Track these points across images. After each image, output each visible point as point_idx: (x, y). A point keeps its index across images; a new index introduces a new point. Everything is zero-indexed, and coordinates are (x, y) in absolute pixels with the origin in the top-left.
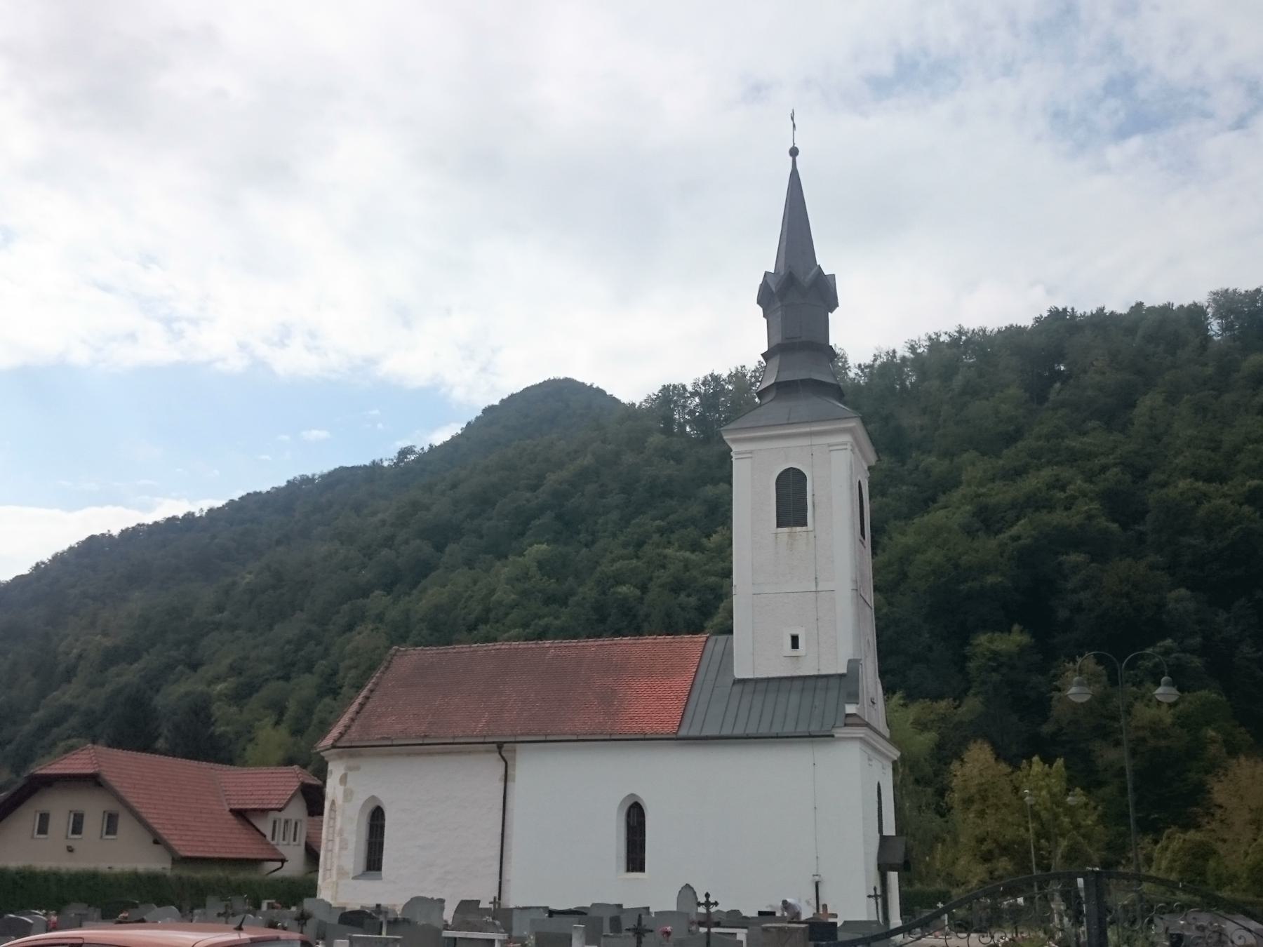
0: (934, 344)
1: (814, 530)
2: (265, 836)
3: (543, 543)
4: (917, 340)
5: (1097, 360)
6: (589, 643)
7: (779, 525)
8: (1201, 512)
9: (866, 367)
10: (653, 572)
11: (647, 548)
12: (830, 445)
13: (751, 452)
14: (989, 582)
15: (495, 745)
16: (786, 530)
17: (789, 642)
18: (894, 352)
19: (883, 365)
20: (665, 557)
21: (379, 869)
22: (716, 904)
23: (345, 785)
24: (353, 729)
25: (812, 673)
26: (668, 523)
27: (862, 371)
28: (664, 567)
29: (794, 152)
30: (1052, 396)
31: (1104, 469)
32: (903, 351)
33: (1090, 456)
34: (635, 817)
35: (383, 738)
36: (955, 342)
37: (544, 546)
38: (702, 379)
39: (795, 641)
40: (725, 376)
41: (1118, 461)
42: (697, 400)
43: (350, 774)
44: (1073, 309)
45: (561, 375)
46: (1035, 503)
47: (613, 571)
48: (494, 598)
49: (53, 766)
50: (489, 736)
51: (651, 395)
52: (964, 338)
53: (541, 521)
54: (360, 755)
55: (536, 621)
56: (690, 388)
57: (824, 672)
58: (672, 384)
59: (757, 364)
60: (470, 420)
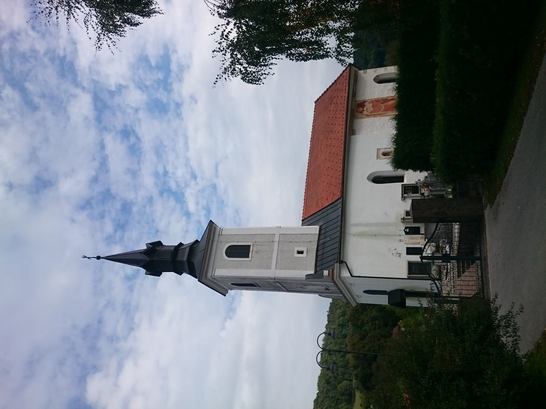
17: (300, 249)
29: (98, 258)
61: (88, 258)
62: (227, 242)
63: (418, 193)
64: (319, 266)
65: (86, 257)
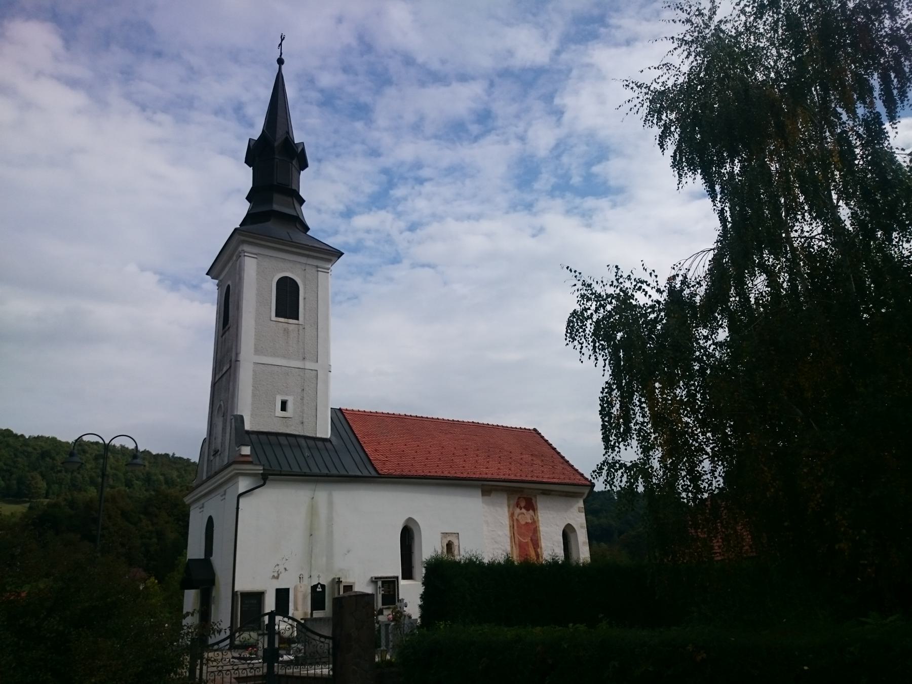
17: (290, 406)
29: (280, 61)
65: (282, 40)
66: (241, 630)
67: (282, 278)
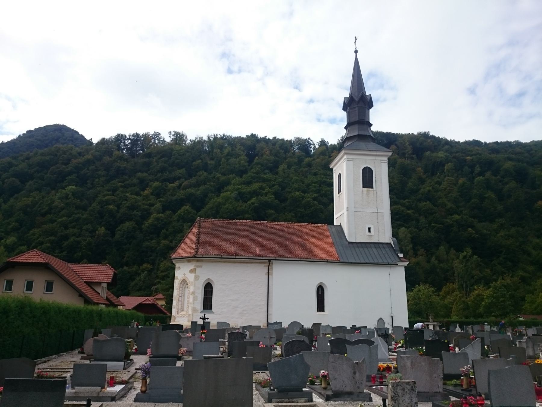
0: (216, 138)
1: (376, 190)
2: (99, 294)
3: (73, 186)
4: (211, 135)
5: (266, 152)
6: (282, 224)
7: (363, 187)
8: (304, 202)
9: (193, 141)
10: (122, 201)
11: (118, 192)
12: (381, 160)
13: (353, 159)
14: (246, 216)
15: (268, 261)
16: (366, 189)
17: (372, 230)
18: (202, 137)
19: (198, 141)
20: (127, 196)
21: (211, 308)
22: (208, 319)
23: (195, 273)
24: (200, 250)
25: (377, 242)
26: (125, 184)
27: (191, 142)
28: (126, 200)
29: (356, 52)
30: (255, 161)
31: (274, 185)
32: (205, 138)
33: (269, 181)
34: (320, 291)
35: (217, 255)
36: (222, 138)
37: (74, 187)
38: (132, 134)
39: (369, 229)
40: (141, 134)
41: (278, 183)
42: (130, 141)
43: (197, 269)
44: (257, 135)
45: (61, 123)
46: (255, 193)
47: (105, 200)
48: (54, 205)
49: (19, 258)
50: (251, 256)
51: (112, 136)
52: (225, 138)
53: (71, 177)
54: (202, 261)
55: (74, 215)
56: (128, 137)
57: (380, 242)
58: (121, 134)
59: (154, 132)
60: (20, 134)
61: (355, 42)
62: (375, 167)
63: (405, 328)
64: (364, 259)
65: (356, 40)
66: (368, 331)
67: (365, 167)
